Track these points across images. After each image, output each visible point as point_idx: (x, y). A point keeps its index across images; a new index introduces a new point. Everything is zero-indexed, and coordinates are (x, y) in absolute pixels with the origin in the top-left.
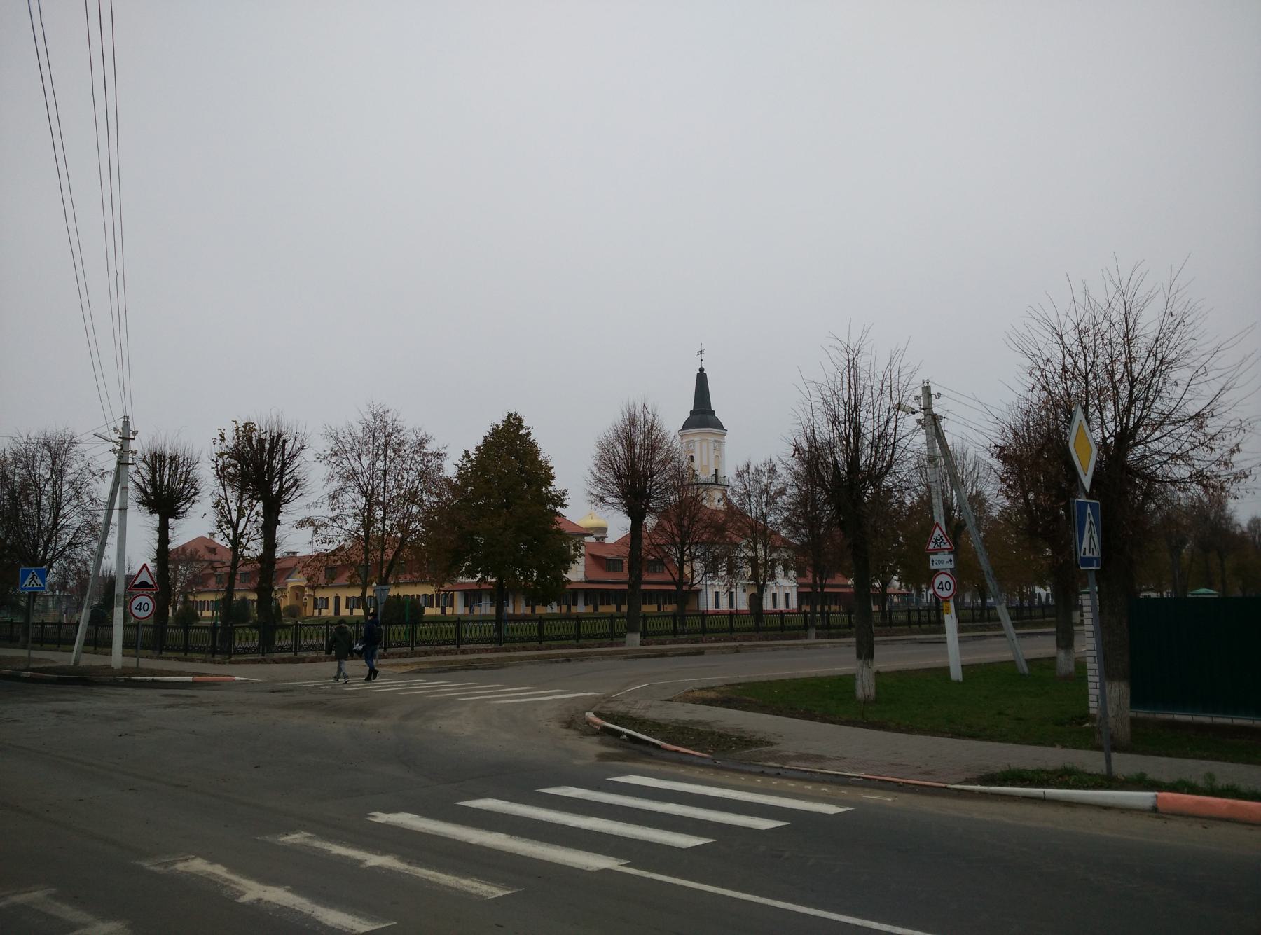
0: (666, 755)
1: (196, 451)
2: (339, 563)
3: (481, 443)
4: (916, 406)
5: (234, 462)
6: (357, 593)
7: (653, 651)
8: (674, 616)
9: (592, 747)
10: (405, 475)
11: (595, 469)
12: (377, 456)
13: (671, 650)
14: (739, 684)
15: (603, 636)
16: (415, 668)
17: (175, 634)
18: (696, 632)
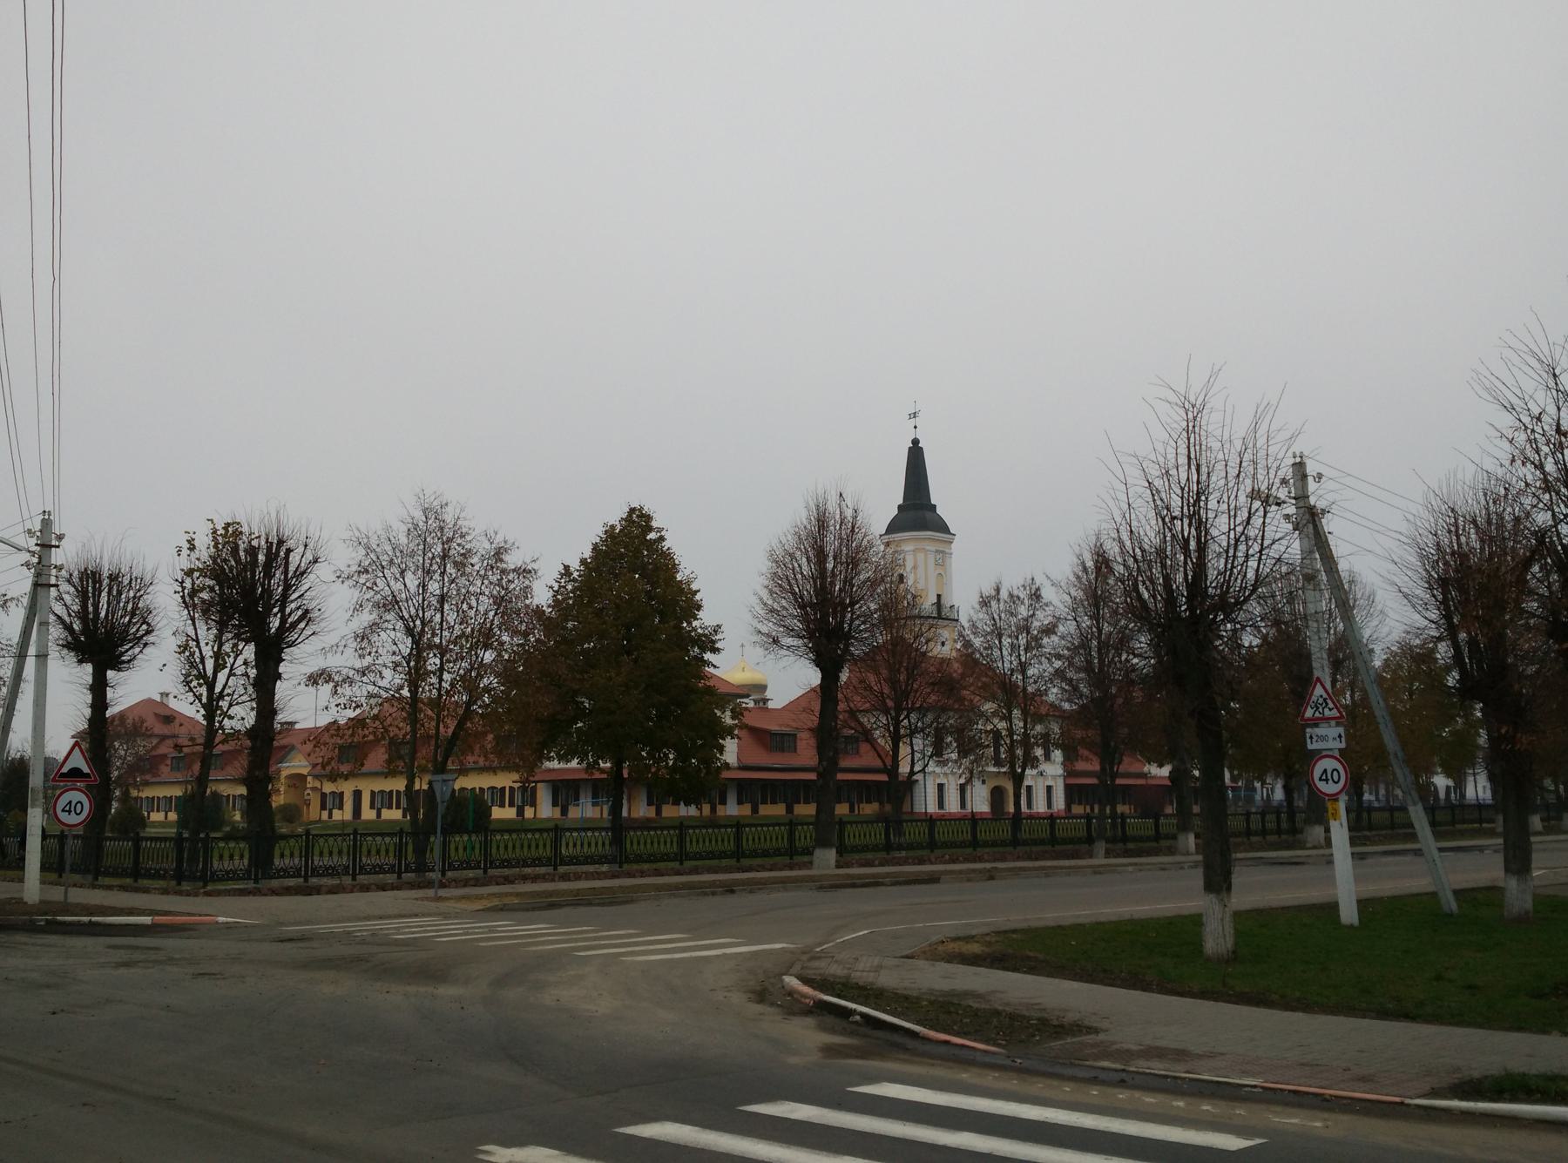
0: (928, 1047)
1: (149, 567)
2: (371, 737)
3: (588, 554)
4: (1282, 494)
5: (212, 583)
6: (399, 784)
7: (860, 877)
8: (880, 818)
9: (808, 1036)
10: (474, 603)
11: (765, 594)
12: (428, 572)
13: (888, 875)
14: (1014, 931)
15: (778, 852)
16: (496, 902)
17: (117, 848)
18: (920, 846)
